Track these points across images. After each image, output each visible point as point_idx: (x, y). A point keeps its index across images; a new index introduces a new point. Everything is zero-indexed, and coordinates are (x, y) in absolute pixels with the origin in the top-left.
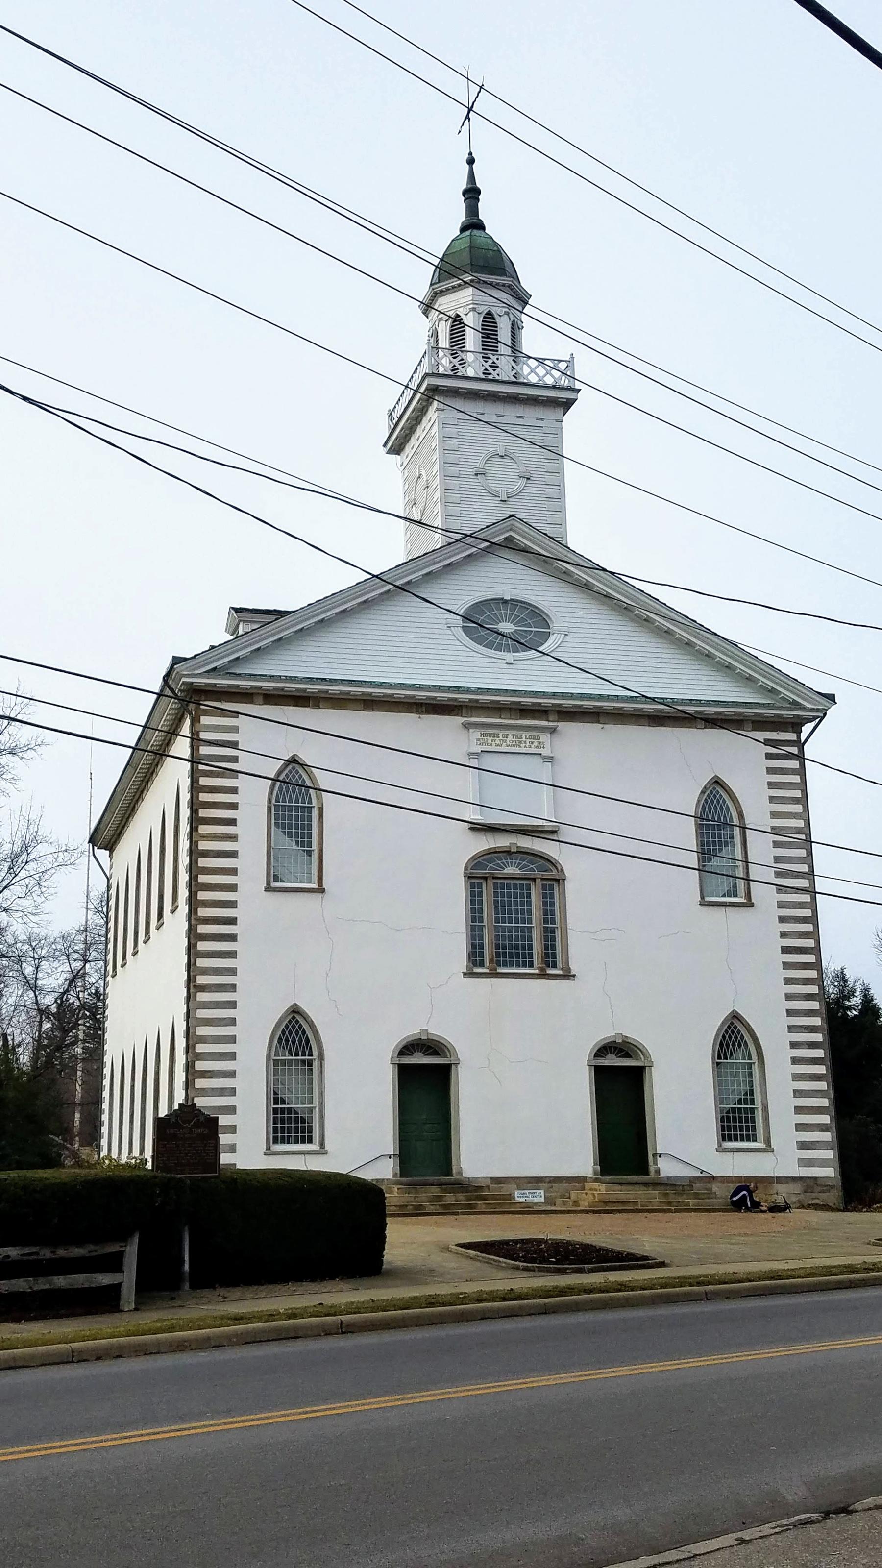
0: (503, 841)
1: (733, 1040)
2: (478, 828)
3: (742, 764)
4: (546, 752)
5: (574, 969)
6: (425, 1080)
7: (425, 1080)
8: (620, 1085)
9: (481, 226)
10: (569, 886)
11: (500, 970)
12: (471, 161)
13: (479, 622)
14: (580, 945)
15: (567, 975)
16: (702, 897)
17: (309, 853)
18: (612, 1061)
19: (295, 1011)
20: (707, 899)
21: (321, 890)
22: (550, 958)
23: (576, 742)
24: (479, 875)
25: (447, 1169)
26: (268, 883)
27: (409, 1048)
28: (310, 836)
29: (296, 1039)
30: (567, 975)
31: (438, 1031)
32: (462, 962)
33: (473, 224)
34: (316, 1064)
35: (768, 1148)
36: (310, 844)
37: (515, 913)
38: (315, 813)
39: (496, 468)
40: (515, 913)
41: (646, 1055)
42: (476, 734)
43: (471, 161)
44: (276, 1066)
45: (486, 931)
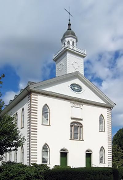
0: (75, 121)
2: (72, 118)
4: (81, 108)
5: (84, 140)
6: (64, 155)
7: (64, 155)
8: (89, 155)
9: (71, 29)
11: (75, 139)
12: (69, 20)
16: (42, 123)
17: (48, 120)
20: (43, 124)
21: (50, 125)
23: (85, 107)
24: (72, 125)
26: (103, 132)
28: (48, 117)
29: (46, 148)
31: (66, 148)
32: (69, 138)
33: (69, 29)
34: (48, 152)
35: (105, 164)
36: (48, 118)
38: (49, 114)
39: (75, 64)
42: (72, 104)
43: (69, 20)
44: (43, 153)
45: (79, 134)
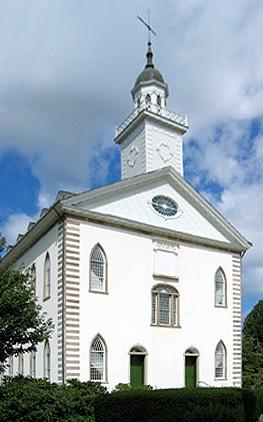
2: (155, 277)
7: (138, 360)
8: (191, 361)
9: (153, 66)
10: (180, 298)
14: (96, 333)
15: (179, 327)
18: (134, 353)
22: (173, 321)
23: (185, 250)
25: (143, 382)
29: (98, 344)
30: (179, 327)
33: (150, 66)
39: (162, 149)
41: (145, 350)
42: (156, 243)
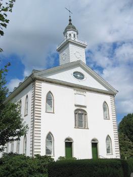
1: (108, 138)
2: (76, 106)
3: (108, 98)
6: (69, 144)
7: (69, 144)
8: (95, 145)
13: (76, 74)
19: (50, 133)
21: (54, 113)
23: (88, 94)
24: (76, 112)
27: (93, 140)
29: (50, 137)
30: (88, 129)
33: (70, 24)
37: (80, 114)
40: (80, 114)
41: (72, 140)
